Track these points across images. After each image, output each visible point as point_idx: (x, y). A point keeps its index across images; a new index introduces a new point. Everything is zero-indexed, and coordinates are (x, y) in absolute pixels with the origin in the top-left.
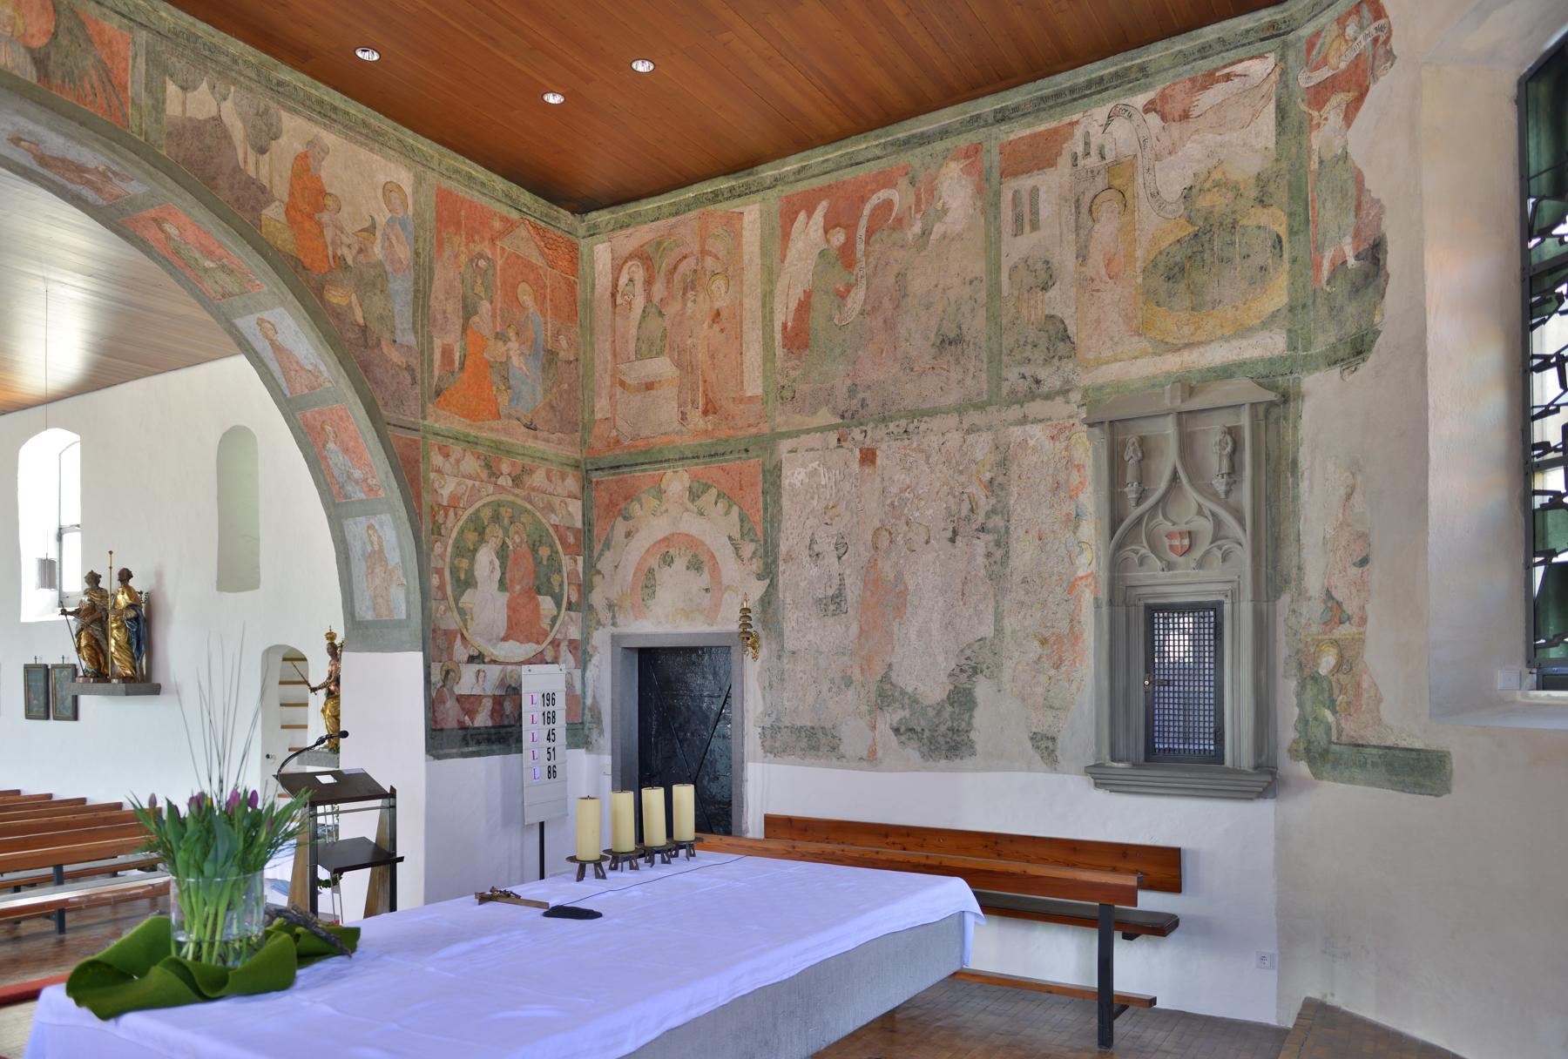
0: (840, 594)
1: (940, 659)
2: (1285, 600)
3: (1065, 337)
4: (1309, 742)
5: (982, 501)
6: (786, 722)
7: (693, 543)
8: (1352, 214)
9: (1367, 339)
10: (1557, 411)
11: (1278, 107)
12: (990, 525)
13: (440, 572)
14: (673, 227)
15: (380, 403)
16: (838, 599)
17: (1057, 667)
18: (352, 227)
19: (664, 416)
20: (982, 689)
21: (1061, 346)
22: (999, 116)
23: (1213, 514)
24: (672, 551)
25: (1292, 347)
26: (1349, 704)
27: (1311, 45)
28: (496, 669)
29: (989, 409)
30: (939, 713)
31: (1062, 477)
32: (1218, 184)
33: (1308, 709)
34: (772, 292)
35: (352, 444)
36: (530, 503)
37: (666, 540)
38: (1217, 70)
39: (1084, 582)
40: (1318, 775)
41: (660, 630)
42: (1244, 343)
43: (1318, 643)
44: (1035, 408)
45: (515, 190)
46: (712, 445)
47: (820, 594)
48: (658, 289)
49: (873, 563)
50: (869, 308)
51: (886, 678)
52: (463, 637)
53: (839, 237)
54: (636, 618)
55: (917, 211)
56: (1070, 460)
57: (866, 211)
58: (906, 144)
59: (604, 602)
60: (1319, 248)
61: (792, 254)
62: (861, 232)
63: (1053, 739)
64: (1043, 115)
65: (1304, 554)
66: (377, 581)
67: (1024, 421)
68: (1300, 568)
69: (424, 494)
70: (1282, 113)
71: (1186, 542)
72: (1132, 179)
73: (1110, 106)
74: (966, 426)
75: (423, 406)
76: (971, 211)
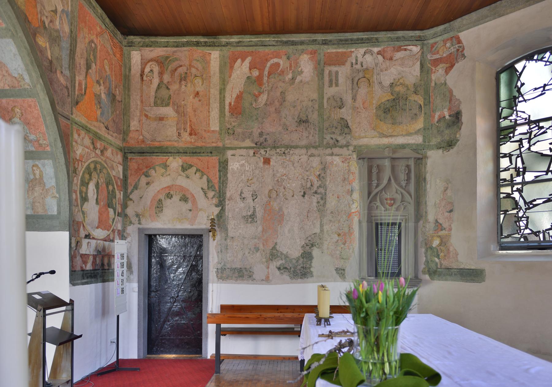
0: (254, 215)
1: (298, 241)
2: (421, 223)
3: (348, 127)
4: (429, 268)
5: (316, 182)
6: (228, 266)
7: (182, 189)
8: (448, 102)
9: (454, 142)
10: (509, 170)
11: (421, 63)
12: (319, 191)
13: (75, 192)
14: (175, 52)
15: (56, 102)
16: (253, 217)
17: (344, 244)
18: (49, 8)
19: (169, 133)
20: (316, 252)
21: (346, 129)
22: (324, 42)
23: (402, 193)
24: (172, 192)
25: (424, 141)
26: (445, 256)
27: (432, 46)
28: (95, 241)
29: (319, 148)
30: (297, 261)
31: (346, 176)
32: (401, 84)
33: (429, 257)
34: (224, 89)
35: (32, 121)
36: (106, 164)
37: (169, 187)
38: (402, 46)
39: (354, 214)
40: (432, 279)
41: (166, 227)
42: (409, 138)
43: (433, 237)
44: (336, 150)
45: (105, 16)
46: (194, 148)
47: (244, 214)
48: (166, 78)
49: (268, 203)
50: (268, 103)
51: (274, 248)
52: (83, 226)
53: (256, 73)
54: (152, 221)
55: (290, 69)
56: (349, 170)
57: (268, 65)
58: (286, 43)
59: (134, 213)
60: (434, 111)
61: (234, 75)
62: (266, 73)
63: (344, 270)
64: (341, 46)
65: (428, 208)
66: (36, 194)
67: (332, 154)
68: (426, 213)
69: (71, 152)
70: (422, 66)
71: (392, 202)
72: (372, 76)
73: (365, 49)
74: (309, 153)
75: (72, 108)
76: (312, 74)
